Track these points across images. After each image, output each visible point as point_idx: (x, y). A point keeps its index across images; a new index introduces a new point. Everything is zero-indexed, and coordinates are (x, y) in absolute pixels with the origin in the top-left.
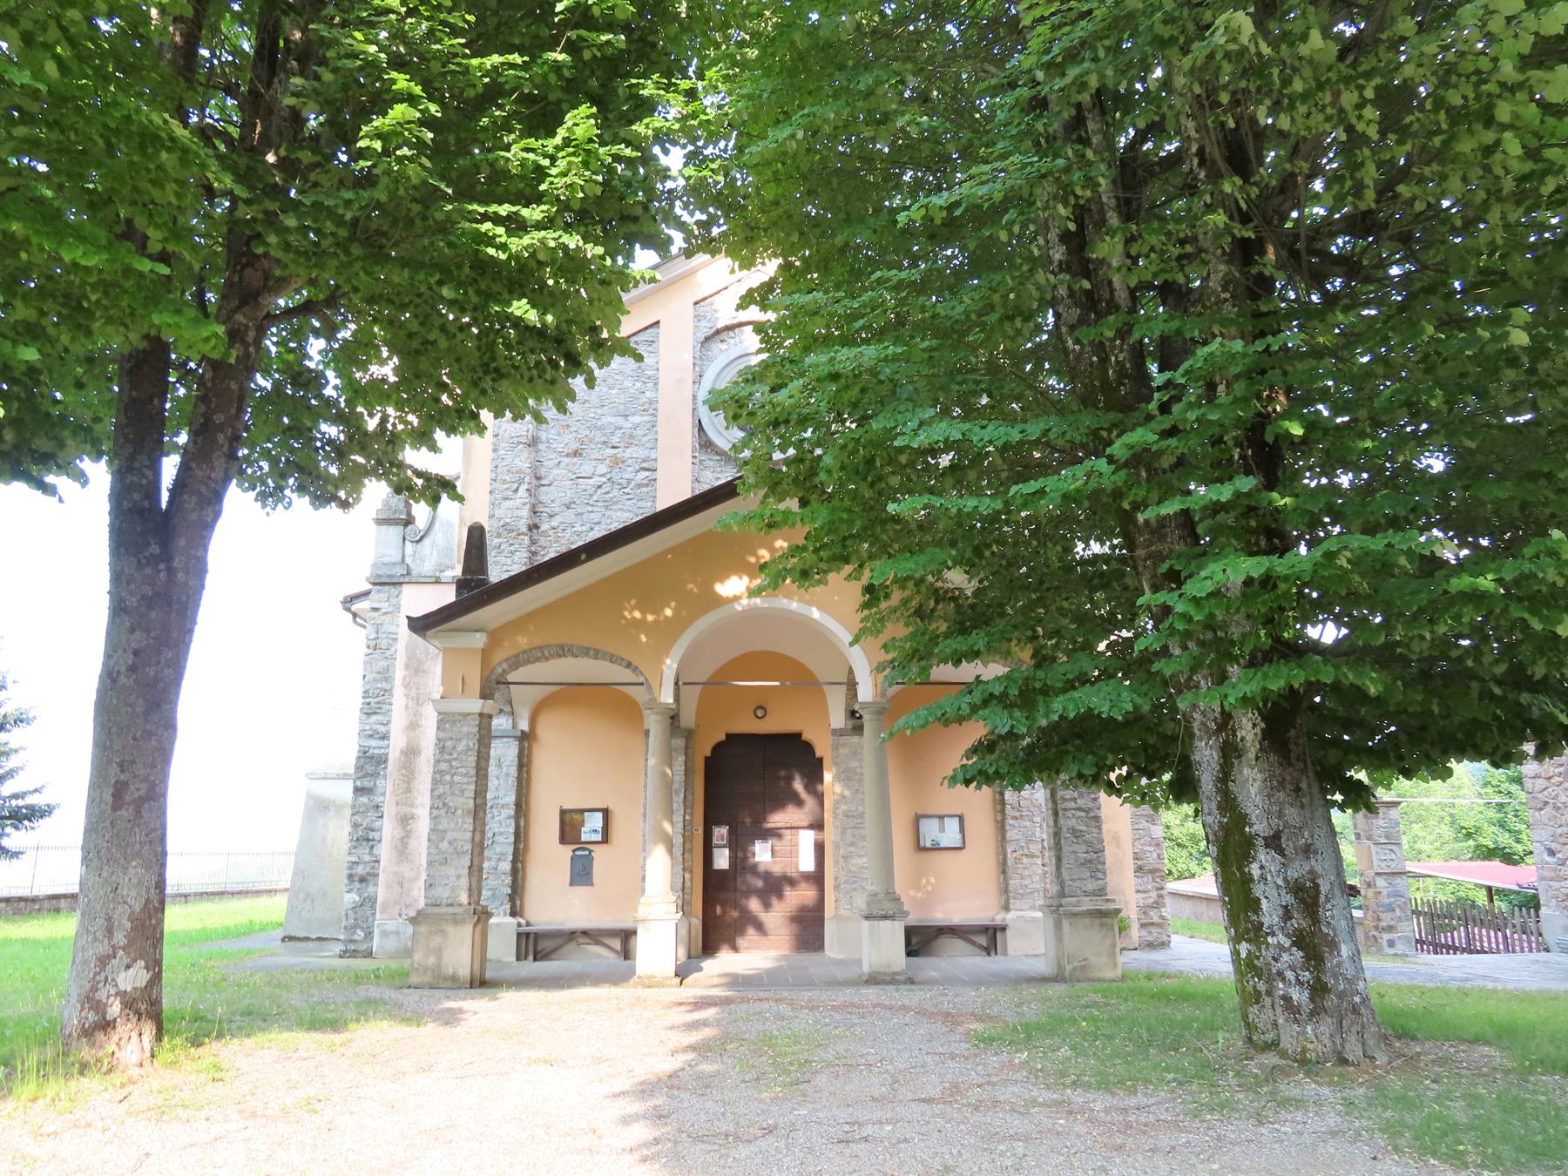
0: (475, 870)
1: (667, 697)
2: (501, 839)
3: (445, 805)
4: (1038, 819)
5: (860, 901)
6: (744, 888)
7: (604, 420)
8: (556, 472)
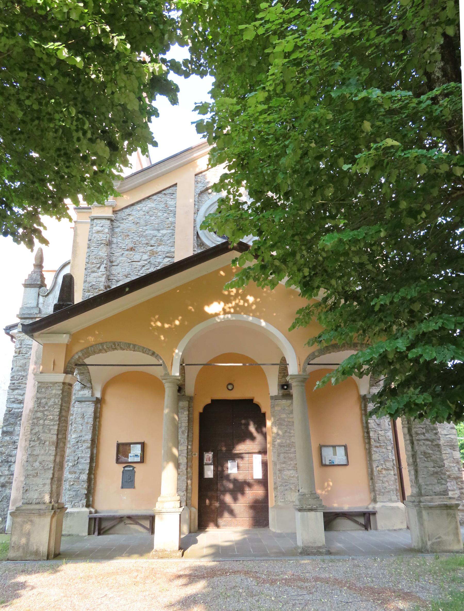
0: (57, 480)
1: (176, 373)
2: (82, 461)
3: (38, 438)
4: (390, 448)
5: (294, 497)
6: (222, 489)
7: (147, 232)
8: (120, 258)
